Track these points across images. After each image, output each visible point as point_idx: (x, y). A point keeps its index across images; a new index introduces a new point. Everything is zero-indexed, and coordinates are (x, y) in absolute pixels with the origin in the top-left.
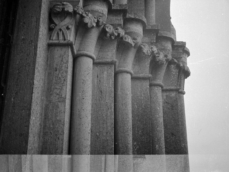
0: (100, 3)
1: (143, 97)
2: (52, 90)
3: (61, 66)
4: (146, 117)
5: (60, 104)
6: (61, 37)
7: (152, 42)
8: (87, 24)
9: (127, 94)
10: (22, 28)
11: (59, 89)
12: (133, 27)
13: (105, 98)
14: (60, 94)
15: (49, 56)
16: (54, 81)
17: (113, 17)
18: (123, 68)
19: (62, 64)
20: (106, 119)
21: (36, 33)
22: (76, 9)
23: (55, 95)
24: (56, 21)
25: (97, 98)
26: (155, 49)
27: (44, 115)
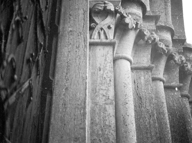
0: (136, 7)
1: (176, 107)
2: (97, 91)
3: (105, 65)
4: (182, 128)
5: (107, 106)
6: (102, 36)
7: (180, 52)
8: (128, 24)
9: (163, 103)
10: (69, 20)
11: (105, 90)
12: (164, 35)
13: (145, 104)
14: (107, 96)
15: (91, 55)
16: (99, 81)
17: (146, 23)
18: (157, 76)
19: (106, 64)
20: (150, 127)
21: (85, 26)
22: (117, 8)
23: (101, 96)
24: (96, 19)
25: (137, 104)
26: (183, 58)
27: (90, 119)
